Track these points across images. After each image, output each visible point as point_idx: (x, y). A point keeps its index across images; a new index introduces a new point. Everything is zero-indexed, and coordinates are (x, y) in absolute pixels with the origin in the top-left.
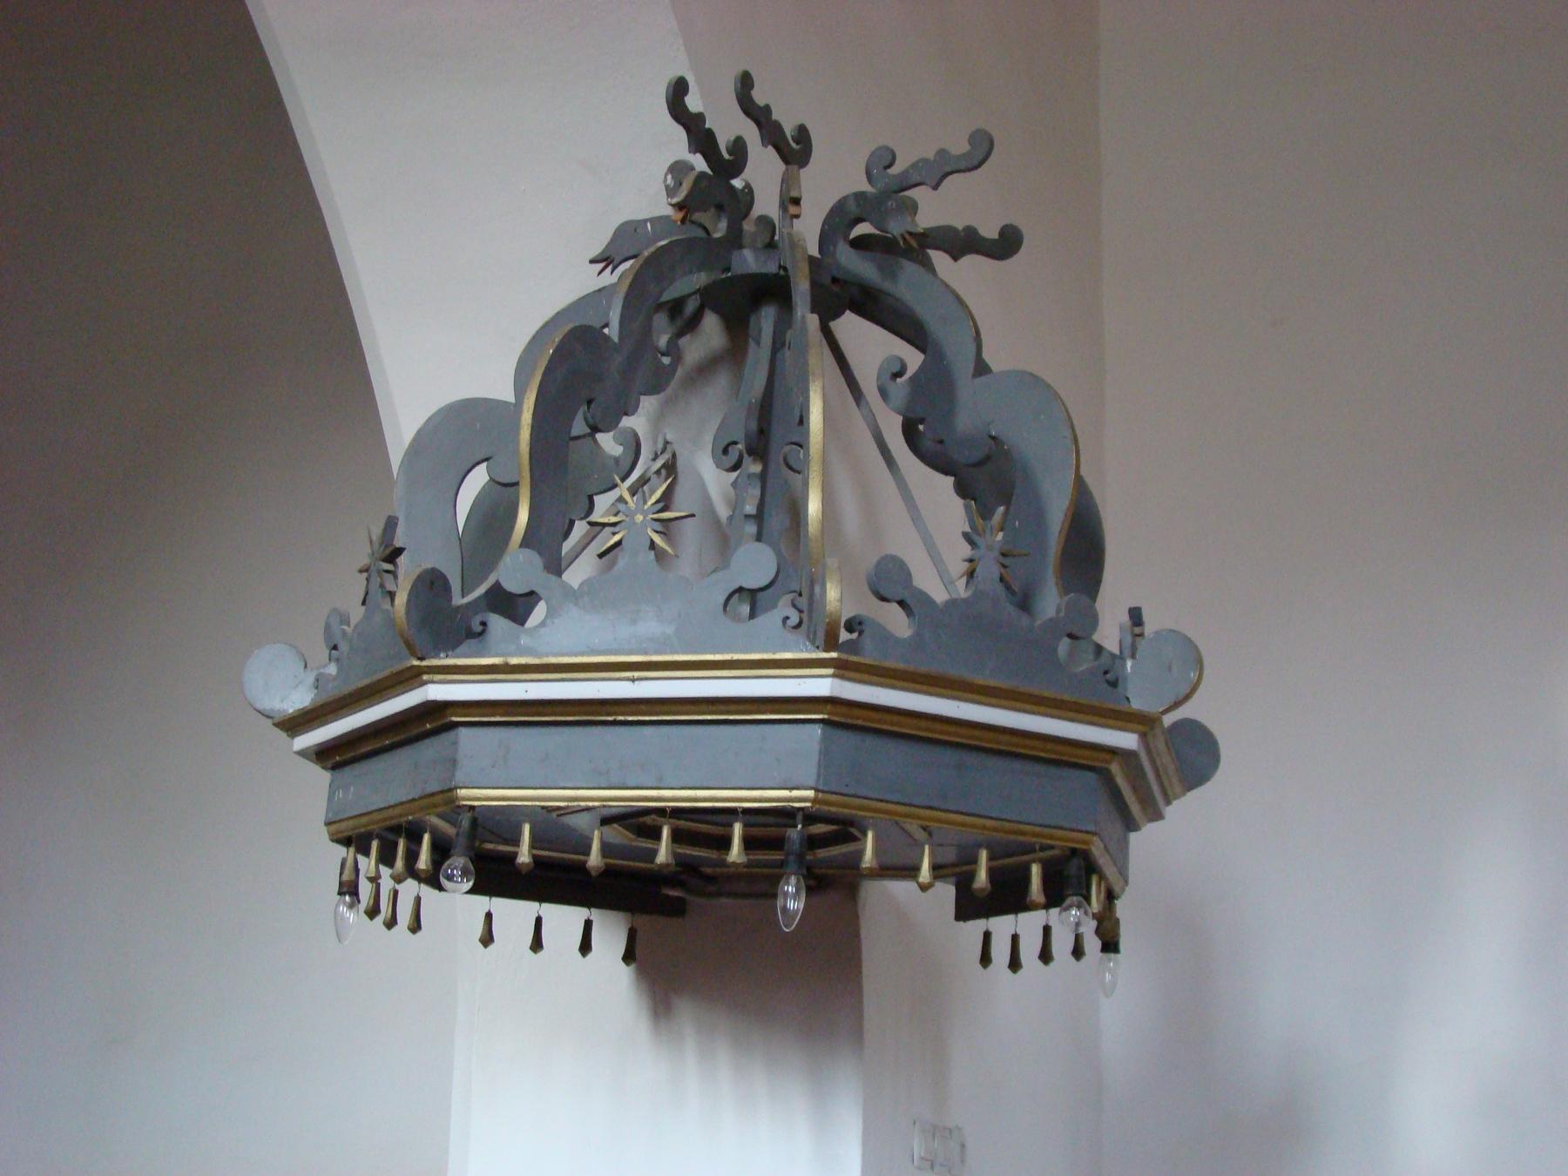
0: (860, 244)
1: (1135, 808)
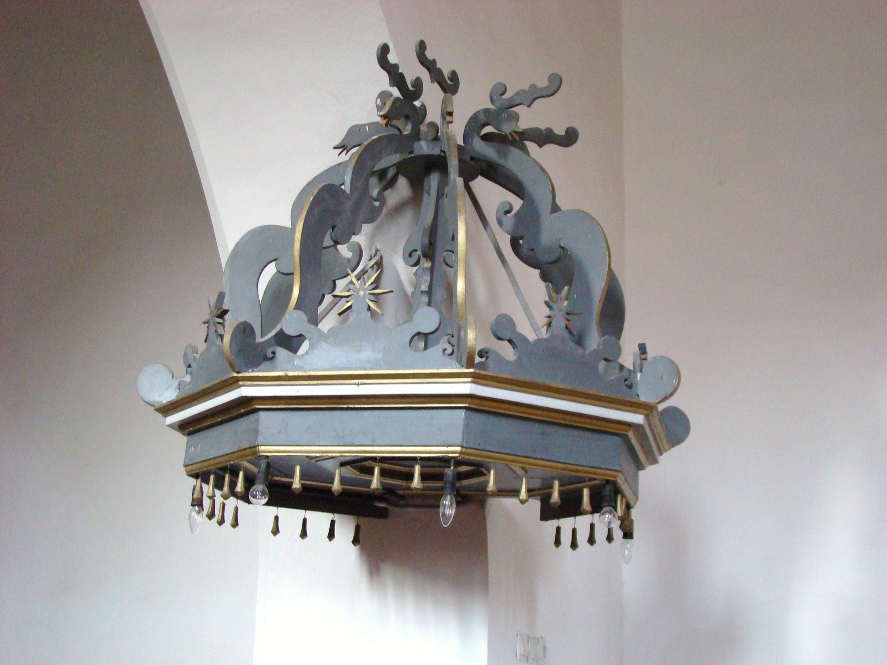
0: (486, 138)
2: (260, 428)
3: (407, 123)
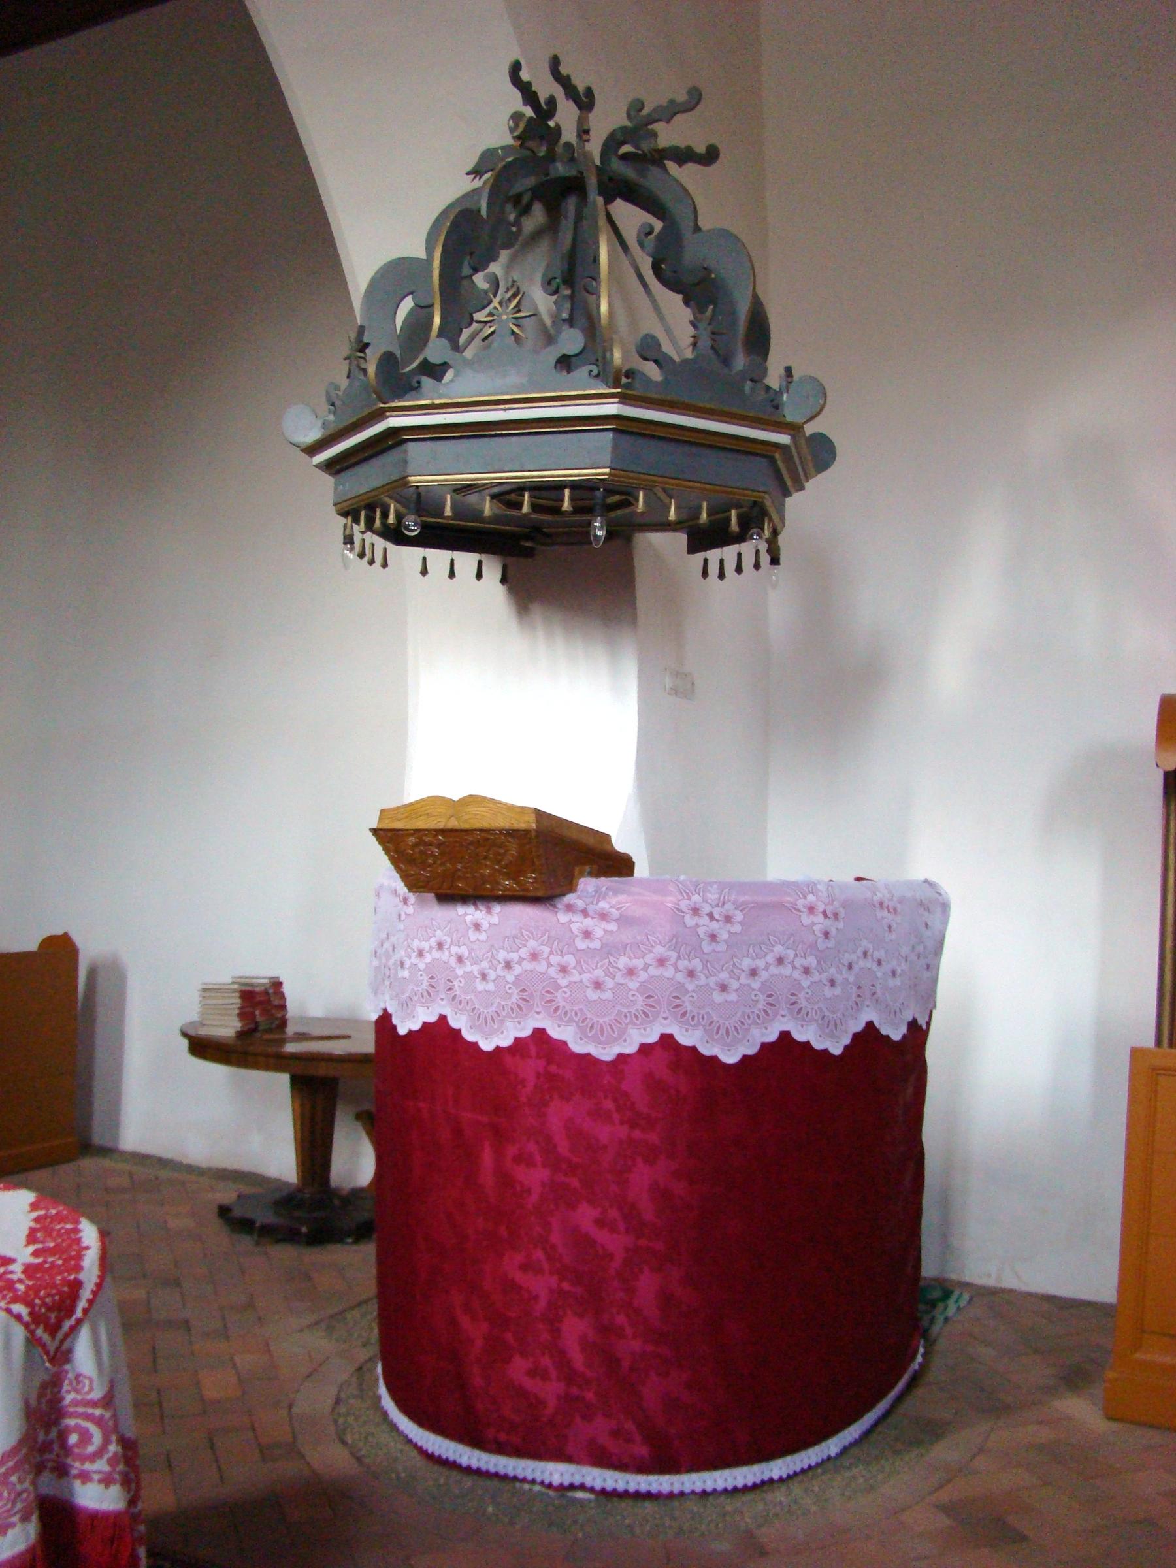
0: (625, 157)
1: (789, 483)
3: (541, 145)
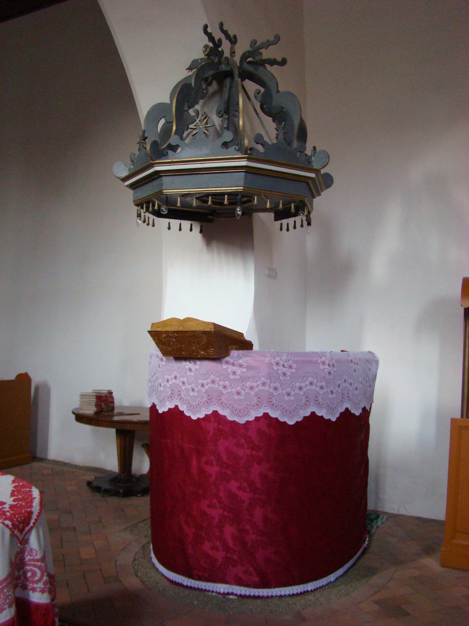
0: (249, 63)
1: (315, 193)
2: (163, 183)
